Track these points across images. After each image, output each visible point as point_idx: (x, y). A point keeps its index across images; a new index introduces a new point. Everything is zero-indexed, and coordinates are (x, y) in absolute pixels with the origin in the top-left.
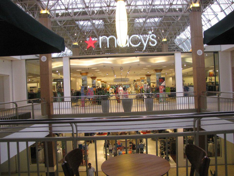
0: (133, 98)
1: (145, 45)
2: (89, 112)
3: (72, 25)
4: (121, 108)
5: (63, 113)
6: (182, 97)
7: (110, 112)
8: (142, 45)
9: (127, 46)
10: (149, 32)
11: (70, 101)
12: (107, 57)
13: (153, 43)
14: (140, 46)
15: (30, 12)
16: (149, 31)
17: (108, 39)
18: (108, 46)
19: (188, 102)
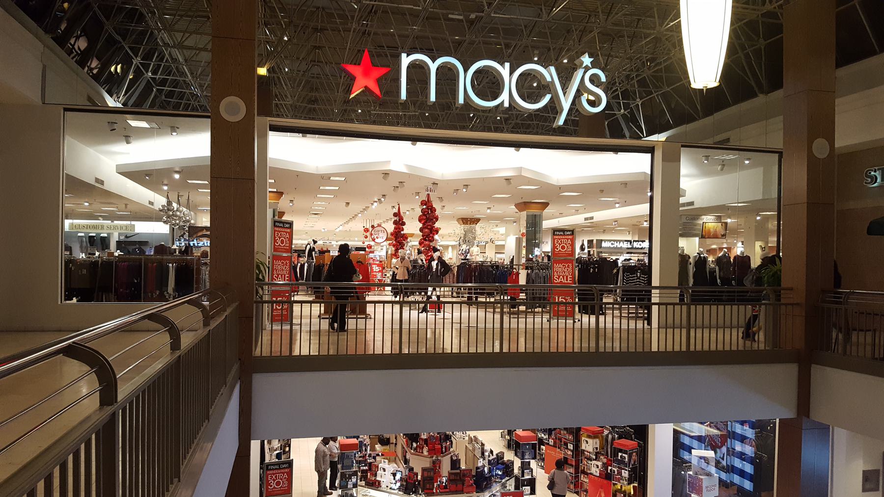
8: (553, 108)
9: (503, 102)
17: (433, 67)
18: (403, 95)
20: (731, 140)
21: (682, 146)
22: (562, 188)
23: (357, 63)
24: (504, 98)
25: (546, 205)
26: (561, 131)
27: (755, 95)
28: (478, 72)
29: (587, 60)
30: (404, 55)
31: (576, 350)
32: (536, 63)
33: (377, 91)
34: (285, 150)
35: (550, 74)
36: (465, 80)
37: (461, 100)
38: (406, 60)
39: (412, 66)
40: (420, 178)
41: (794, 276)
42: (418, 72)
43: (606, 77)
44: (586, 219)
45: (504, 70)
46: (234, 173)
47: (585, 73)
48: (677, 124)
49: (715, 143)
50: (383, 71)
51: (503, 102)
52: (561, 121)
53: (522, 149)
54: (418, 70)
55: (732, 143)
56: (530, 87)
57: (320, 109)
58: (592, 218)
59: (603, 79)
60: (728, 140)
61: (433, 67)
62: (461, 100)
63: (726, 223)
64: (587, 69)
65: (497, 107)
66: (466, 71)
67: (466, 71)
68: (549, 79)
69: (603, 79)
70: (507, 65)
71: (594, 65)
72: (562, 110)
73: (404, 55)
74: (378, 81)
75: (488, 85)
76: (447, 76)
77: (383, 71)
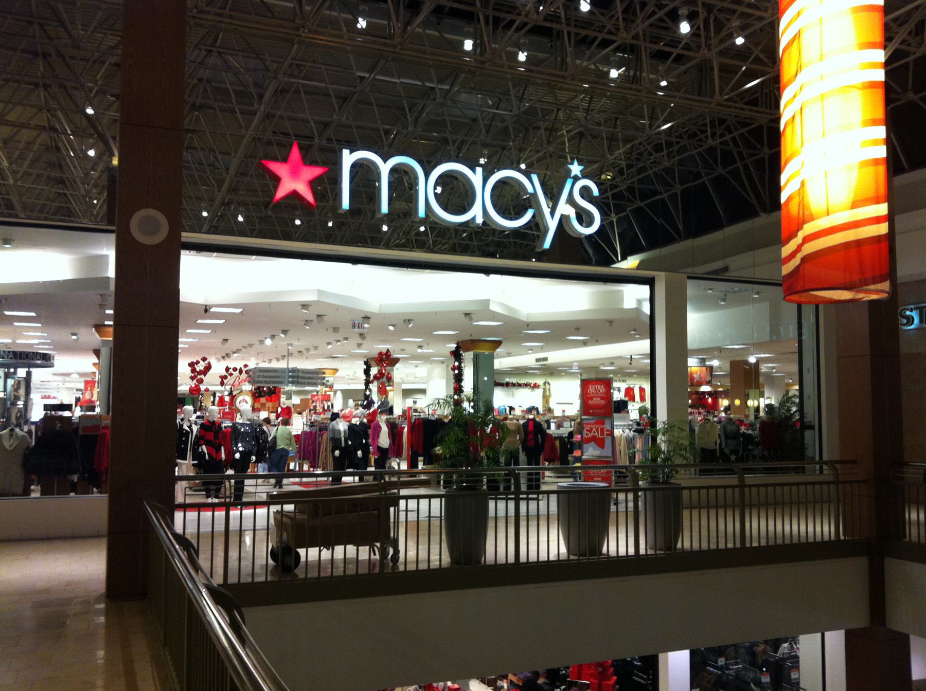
0: (683, 485)
1: (552, 225)
2: (706, 545)
3: (393, 76)
4: (435, 539)
5: (533, 558)
6: (697, 491)
7: (679, 545)
8: (537, 225)
9: (474, 219)
10: (571, 167)
11: (736, 486)
12: (487, 271)
13: (583, 217)
14: (527, 225)
15: (675, 52)
16: (572, 163)
17: (385, 168)
18: (346, 204)
19: (523, 524)
20: (731, 268)
21: (689, 278)
22: (529, 325)
23: (285, 160)
24: (475, 214)
25: (498, 344)
26: (543, 256)
27: (755, 214)
28: (502, 183)
29: (576, 169)
30: (346, 152)
31: (551, 558)
32: (520, 171)
33: (310, 197)
34: (207, 279)
35: (533, 185)
36: (427, 190)
37: (422, 213)
38: (348, 158)
39: (357, 167)
40: (350, 310)
41: (826, 442)
42: (364, 174)
43: (599, 190)
44: (538, 360)
45: (476, 177)
46: (144, 320)
47: (573, 184)
48: (652, 246)
49: (708, 273)
50: (317, 171)
51: (474, 219)
52: (547, 245)
53: (492, 276)
54: (364, 172)
55: (732, 274)
56: (509, 199)
57: (71, 195)
58: (545, 359)
59: (596, 192)
60: (726, 269)
61: (385, 168)
62: (422, 213)
63: (711, 368)
64: (576, 179)
65: (466, 224)
66: (427, 176)
67: (427, 176)
68: (530, 189)
69: (596, 192)
70: (479, 170)
71: (585, 176)
72: (546, 231)
73: (346, 152)
74: (312, 184)
75: (456, 194)
76: (403, 183)
77: (317, 171)
